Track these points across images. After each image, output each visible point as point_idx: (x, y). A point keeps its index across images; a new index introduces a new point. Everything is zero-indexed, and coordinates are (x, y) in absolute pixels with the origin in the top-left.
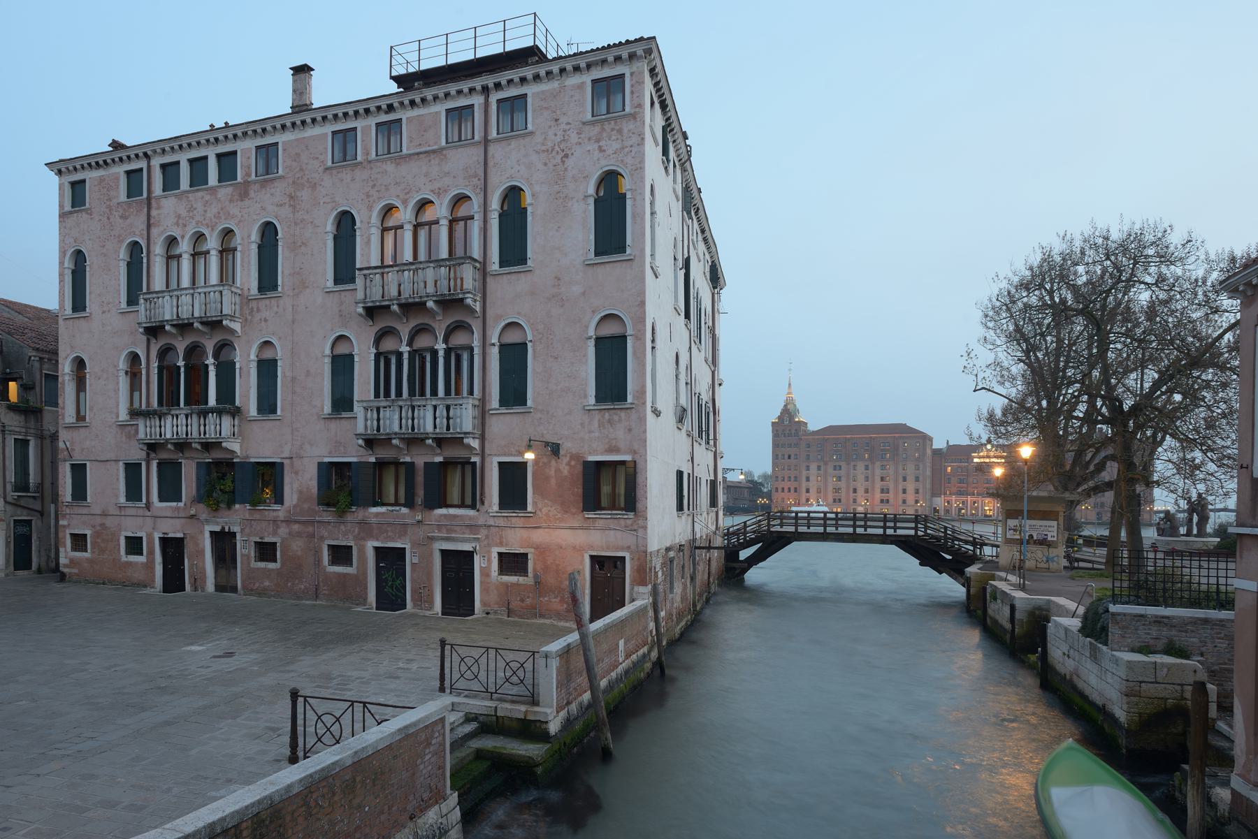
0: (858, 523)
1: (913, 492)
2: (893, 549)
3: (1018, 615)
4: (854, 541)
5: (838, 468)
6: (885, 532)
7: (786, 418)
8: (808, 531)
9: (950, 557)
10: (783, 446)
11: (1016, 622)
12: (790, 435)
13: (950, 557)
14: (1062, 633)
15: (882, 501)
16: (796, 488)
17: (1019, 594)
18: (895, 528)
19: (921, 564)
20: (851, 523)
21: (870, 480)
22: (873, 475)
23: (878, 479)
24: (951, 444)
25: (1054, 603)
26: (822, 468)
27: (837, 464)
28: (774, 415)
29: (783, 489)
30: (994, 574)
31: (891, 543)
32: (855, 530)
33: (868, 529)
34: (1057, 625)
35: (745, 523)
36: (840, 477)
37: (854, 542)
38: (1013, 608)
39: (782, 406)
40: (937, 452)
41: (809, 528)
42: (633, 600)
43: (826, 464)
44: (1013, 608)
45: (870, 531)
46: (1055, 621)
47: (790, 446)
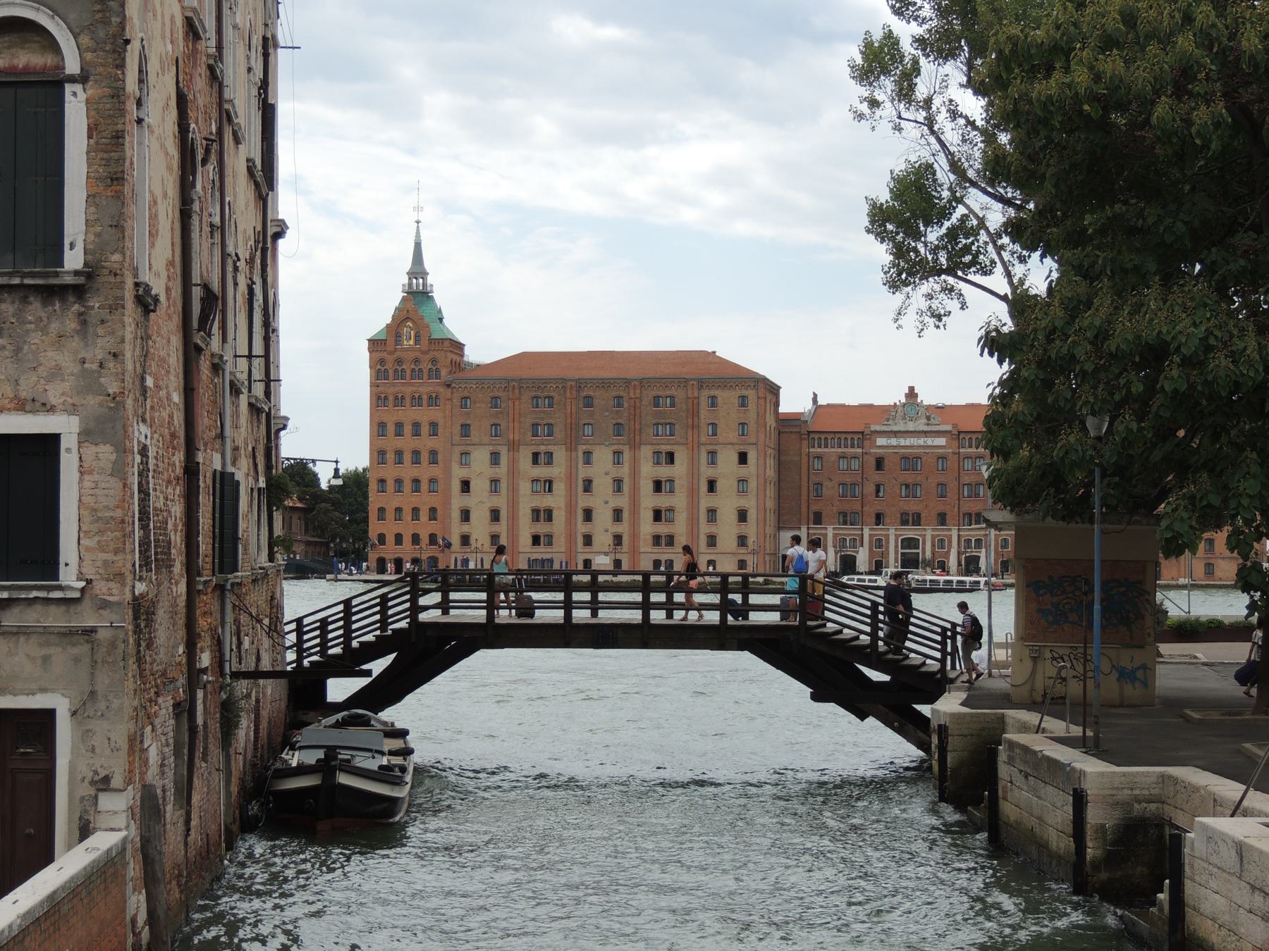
0: (576, 596)
1: (734, 517)
2: (746, 660)
3: (1095, 816)
4: (645, 645)
5: (542, 458)
6: (646, 616)
7: (408, 330)
8: (594, 621)
9: (886, 678)
10: (399, 401)
11: (1089, 833)
12: (417, 374)
13: (886, 678)
14: (1228, 857)
15: (657, 540)
16: (433, 511)
17: (1091, 767)
18: (594, 606)
19: (816, 697)
20: (637, 597)
21: (626, 487)
22: (635, 474)
23: (646, 487)
24: (821, 401)
25: (1175, 781)
26: (504, 459)
27: (542, 448)
28: (380, 317)
29: (399, 510)
30: (1003, 715)
31: (741, 647)
32: (568, 616)
33: (601, 613)
34: (1212, 837)
35: (347, 603)
36: (550, 482)
37: (645, 645)
38: (1080, 800)
39: (395, 298)
40: (790, 424)
41: (446, 612)
42: (85, 831)
43: (514, 446)
44: (1080, 800)
45: (605, 616)
46: (1205, 827)
47: (417, 401)
